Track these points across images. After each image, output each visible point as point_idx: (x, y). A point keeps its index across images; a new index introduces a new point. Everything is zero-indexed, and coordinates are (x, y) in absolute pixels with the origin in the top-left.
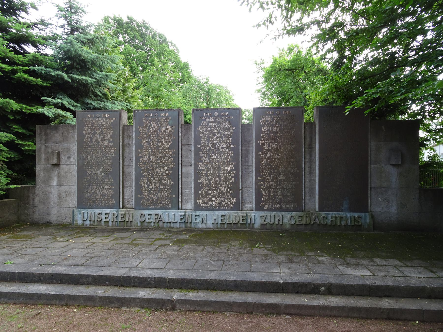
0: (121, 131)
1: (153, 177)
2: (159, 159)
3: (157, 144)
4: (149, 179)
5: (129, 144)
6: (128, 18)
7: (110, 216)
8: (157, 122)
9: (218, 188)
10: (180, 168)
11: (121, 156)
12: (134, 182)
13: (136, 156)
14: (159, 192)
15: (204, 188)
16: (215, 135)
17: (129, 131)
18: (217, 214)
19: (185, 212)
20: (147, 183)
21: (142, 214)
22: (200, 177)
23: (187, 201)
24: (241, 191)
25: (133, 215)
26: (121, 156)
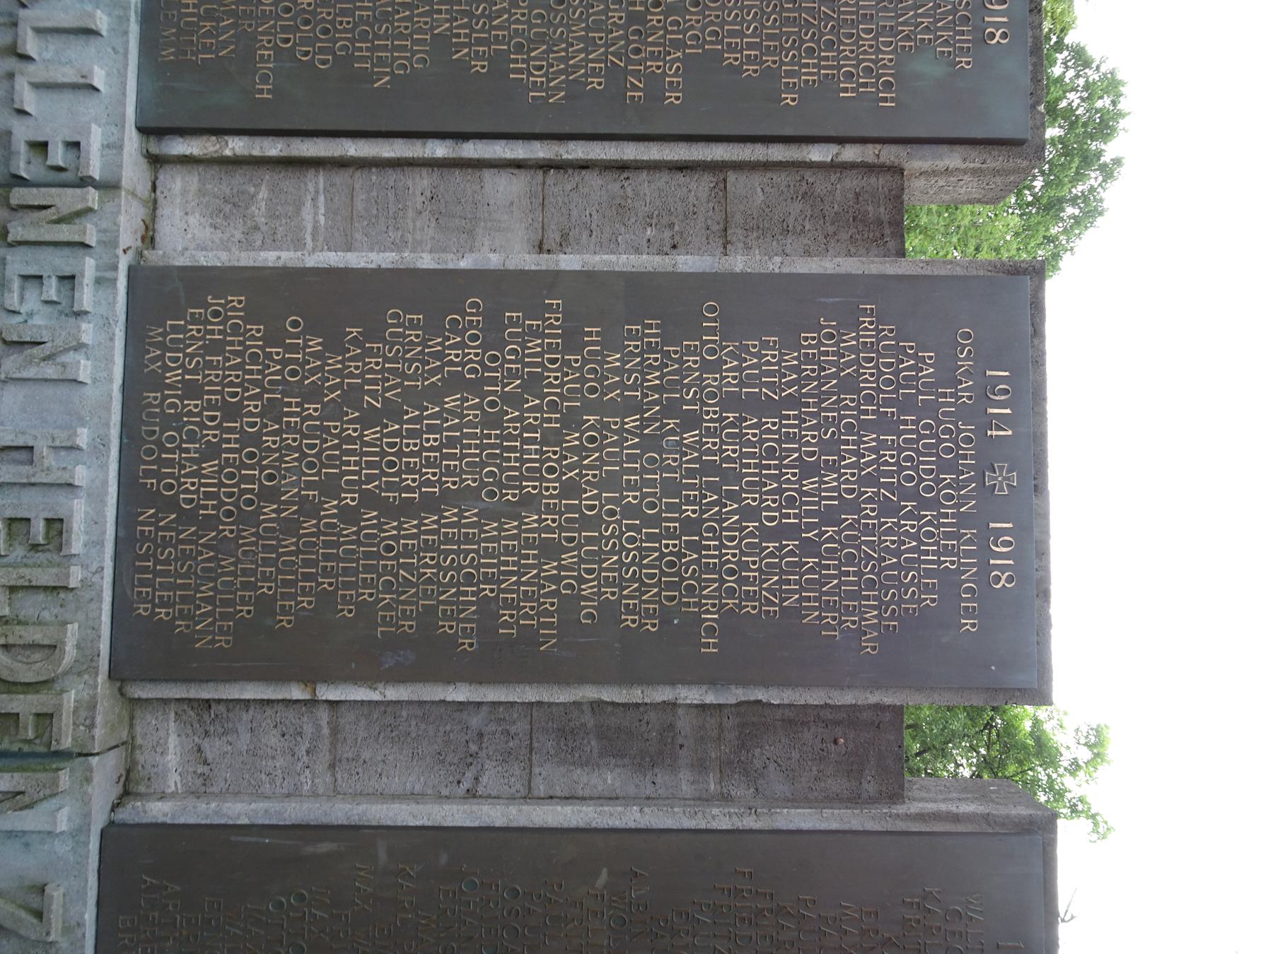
6: (1117, 162)
9: (330, 488)
10: (518, 151)
15: (334, 363)
16: (808, 470)
18: (81, 475)
19: (109, 187)
22: (433, 327)
23: (228, 209)
24: (297, 692)
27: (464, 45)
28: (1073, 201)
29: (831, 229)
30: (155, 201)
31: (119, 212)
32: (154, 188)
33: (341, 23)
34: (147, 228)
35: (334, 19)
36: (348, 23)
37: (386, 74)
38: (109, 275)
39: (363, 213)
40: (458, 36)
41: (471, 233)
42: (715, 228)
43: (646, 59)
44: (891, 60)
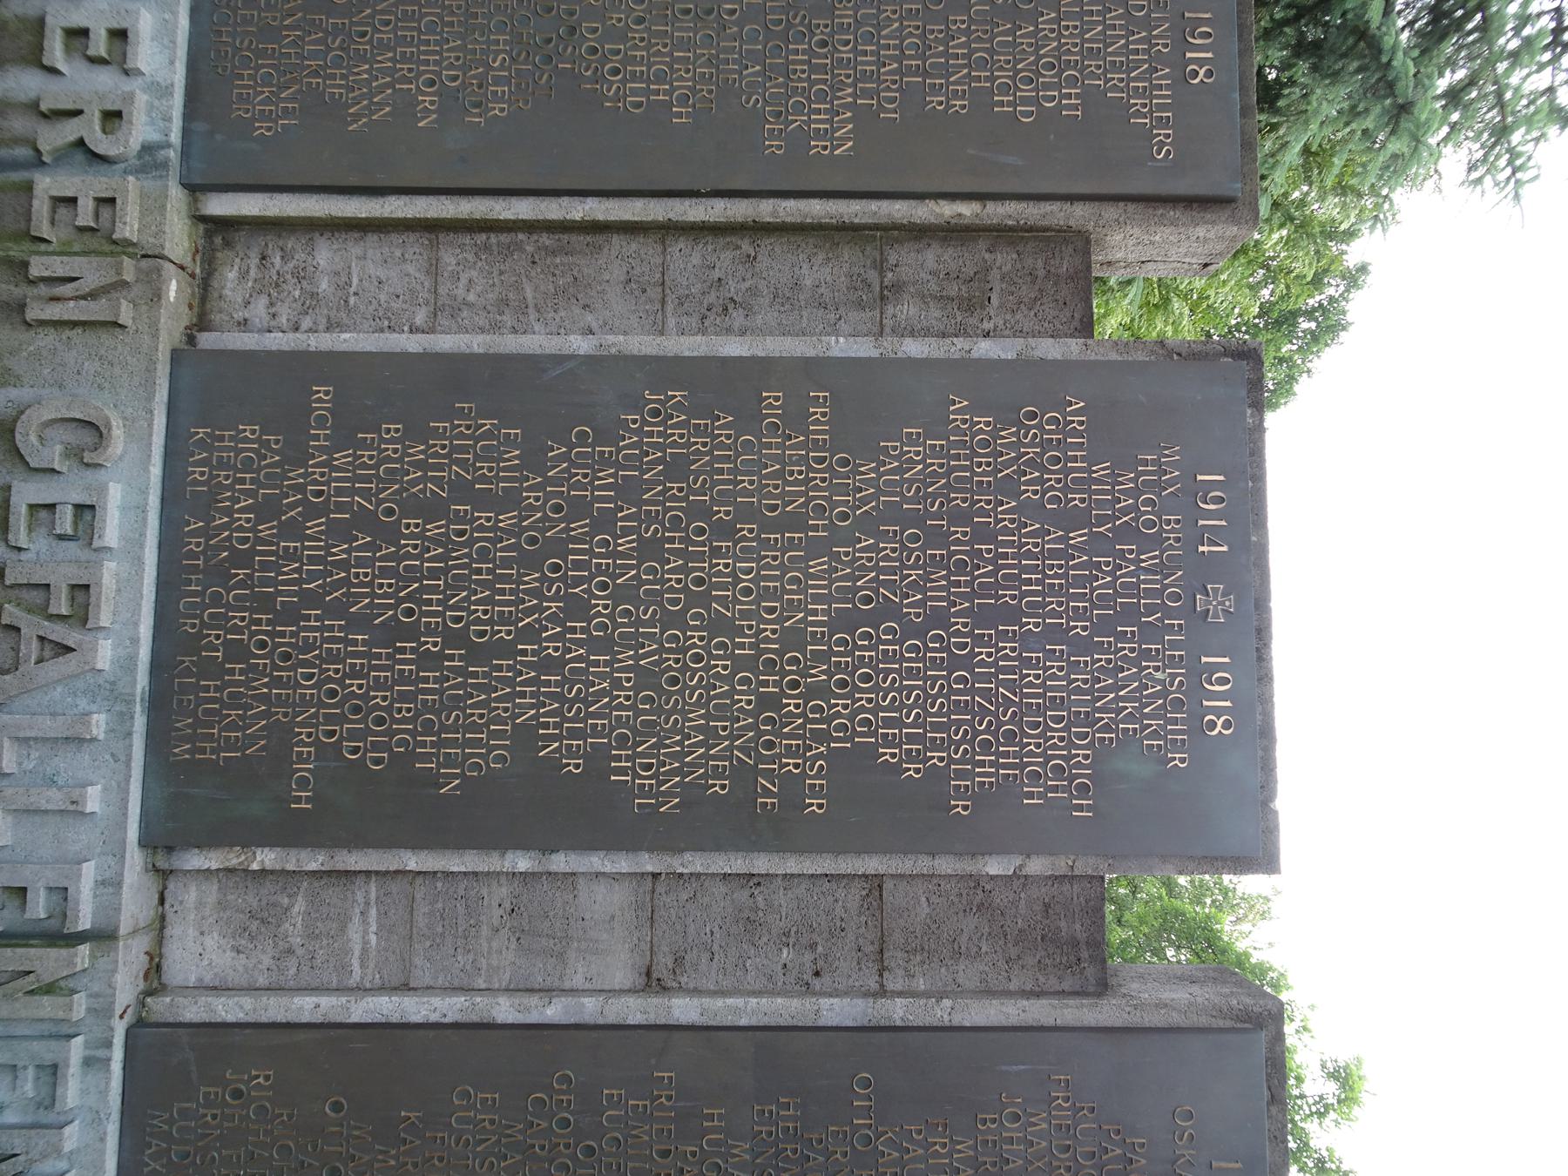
0: (1031, 213)
1: (529, 562)
2: (717, 626)
3: (890, 611)
4: (506, 520)
5: (889, 293)
6: (1363, 269)
7: (105, 79)
8: (1130, 614)
11: (766, 210)
12: (476, 343)
13: (762, 368)
14: (356, 623)
17: (1028, 293)
20: (461, 490)
21: (96, 430)
23: (255, 909)
25: (106, 338)
26: (766, 210)
27: (554, 738)
28: (1309, 314)
29: (1014, 952)
30: (163, 918)
31: (115, 971)
32: (162, 901)
33: (400, 710)
34: (152, 959)
35: (391, 705)
36: (409, 710)
37: (455, 776)
38: (101, 1053)
39: (425, 931)
40: (546, 726)
41: (561, 956)
42: (869, 949)
43: (780, 756)
44: (1086, 757)
